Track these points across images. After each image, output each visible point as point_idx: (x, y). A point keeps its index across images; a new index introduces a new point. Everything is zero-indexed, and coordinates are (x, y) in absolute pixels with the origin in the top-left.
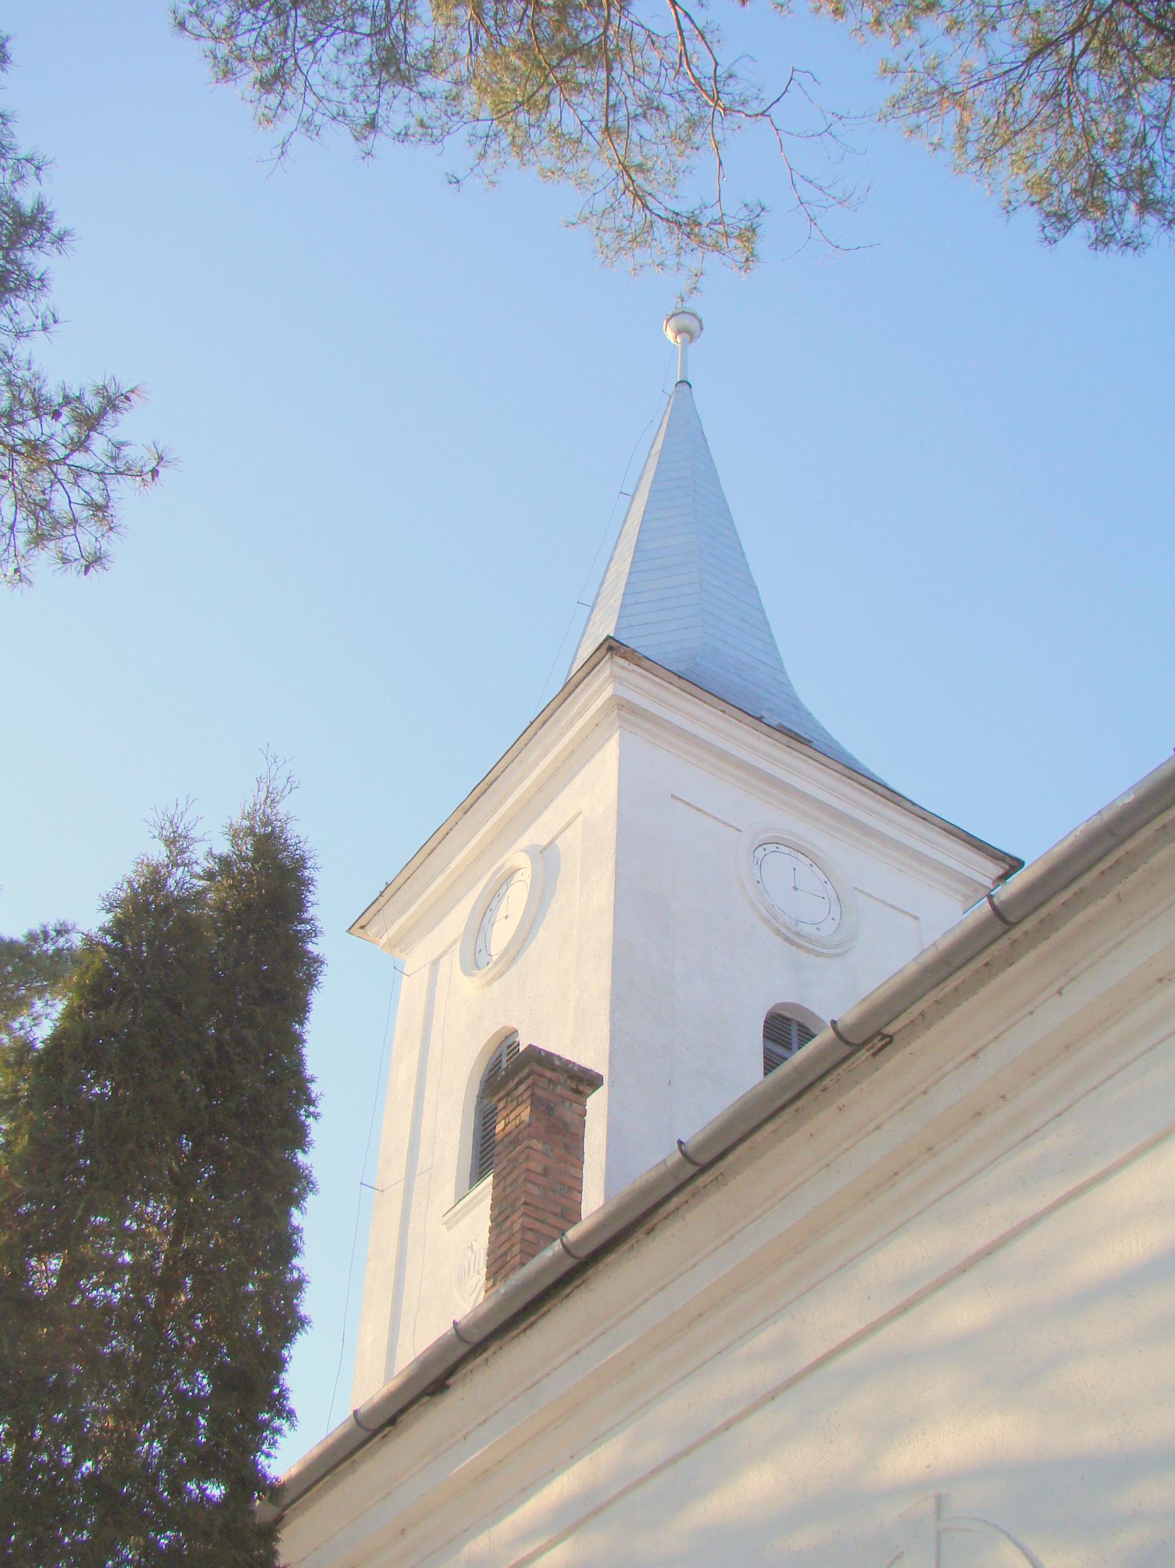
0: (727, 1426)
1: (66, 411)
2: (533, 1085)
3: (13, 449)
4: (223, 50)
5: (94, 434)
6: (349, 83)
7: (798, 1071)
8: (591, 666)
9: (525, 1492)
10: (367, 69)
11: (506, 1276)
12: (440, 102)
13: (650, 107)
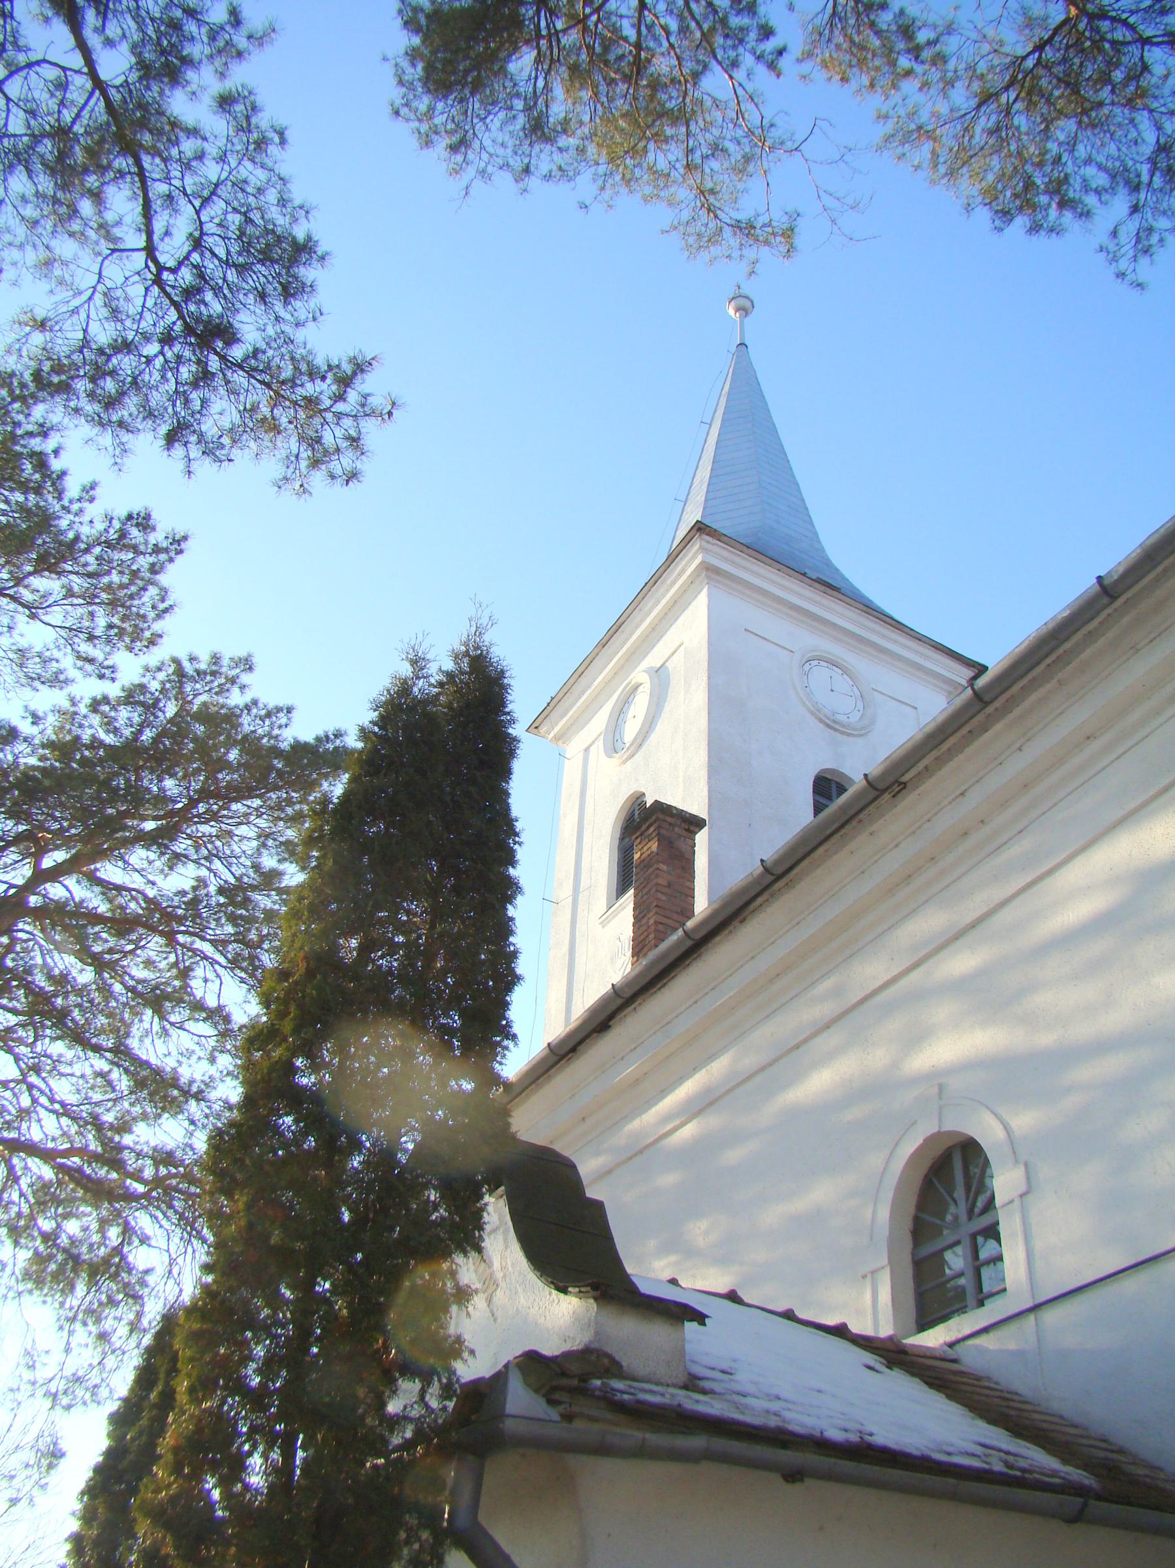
0: (797, 1047)
1: (330, 376)
2: (659, 827)
3: (295, 403)
4: (424, 128)
5: (349, 390)
6: (510, 143)
7: (843, 808)
8: (686, 541)
9: (664, 1092)
10: (521, 134)
11: (645, 954)
12: (572, 152)
13: (717, 149)
